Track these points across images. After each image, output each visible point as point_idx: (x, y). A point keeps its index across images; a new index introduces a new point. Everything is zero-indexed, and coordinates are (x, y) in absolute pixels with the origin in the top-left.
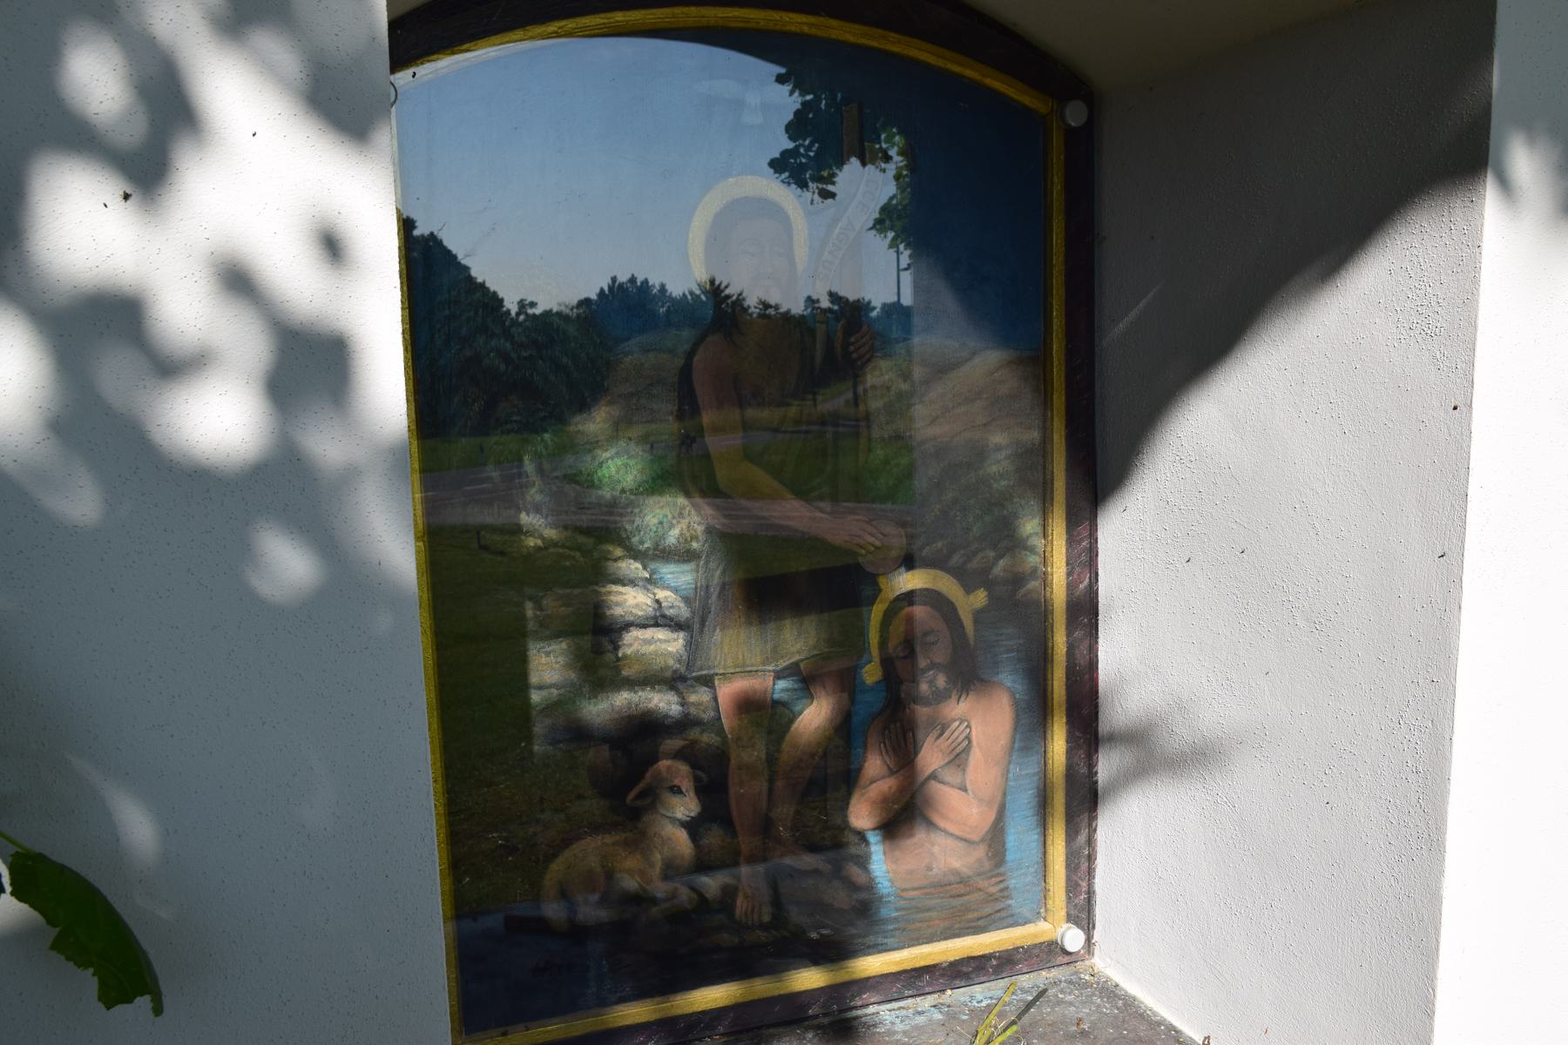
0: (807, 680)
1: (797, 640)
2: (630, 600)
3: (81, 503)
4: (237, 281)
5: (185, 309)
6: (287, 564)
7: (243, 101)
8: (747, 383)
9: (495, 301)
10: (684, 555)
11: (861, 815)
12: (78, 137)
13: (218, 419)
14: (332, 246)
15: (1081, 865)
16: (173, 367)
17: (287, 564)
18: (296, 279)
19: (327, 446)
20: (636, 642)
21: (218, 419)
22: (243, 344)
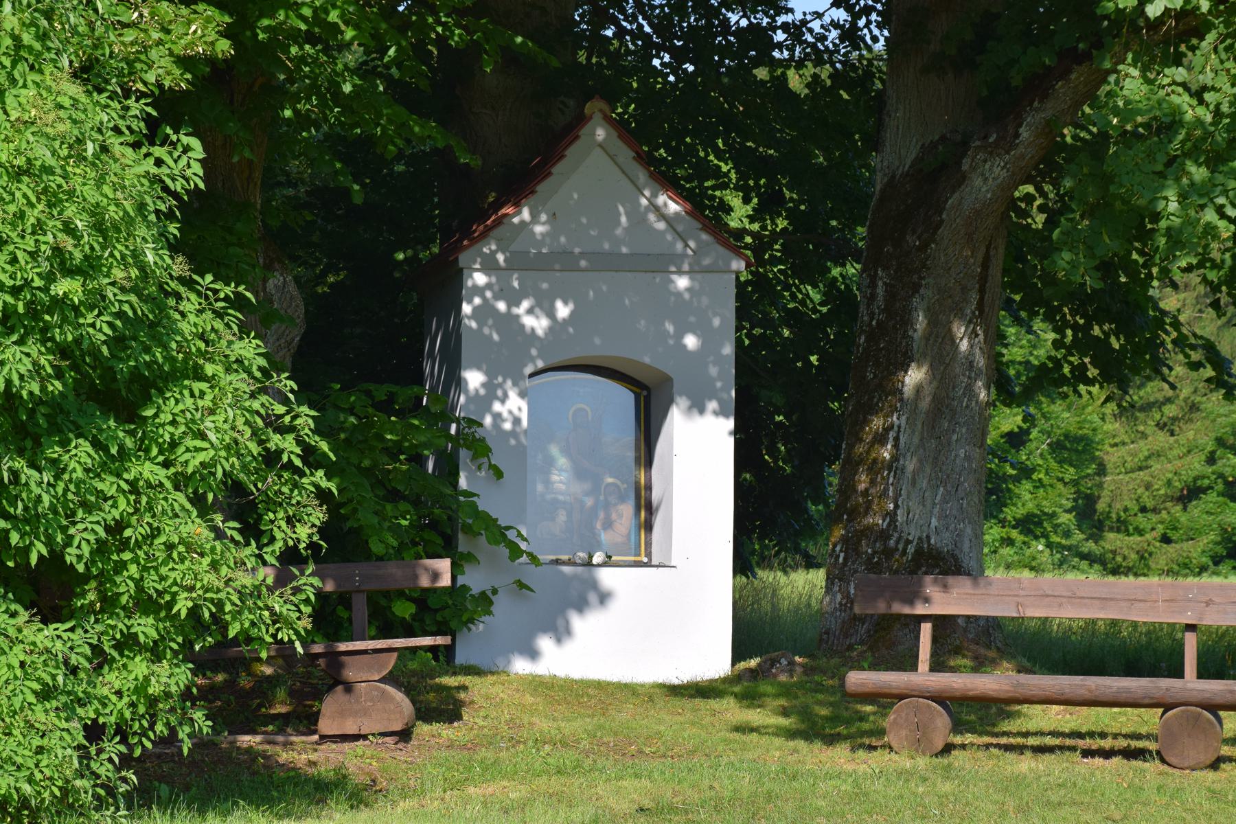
0: (587, 494)
1: (587, 486)
2: (555, 478)
3: (494, 433)
4: (510, 412)
5: (505, 415)
6: (513, 442)
7: (513, 395)
8: (851, 544)
9: (737, 431)
10: (565, 471)
11: (598, 526)
12: (497, 398)
13: (507, 426)
14: (520, 409)
15: (649, 544)
16: (504, 420)
17: (513, 442)
18: (516, 412)
19: (518, 429)
20: (556, 485)
21: (507, 426)
22: (510, 418)
